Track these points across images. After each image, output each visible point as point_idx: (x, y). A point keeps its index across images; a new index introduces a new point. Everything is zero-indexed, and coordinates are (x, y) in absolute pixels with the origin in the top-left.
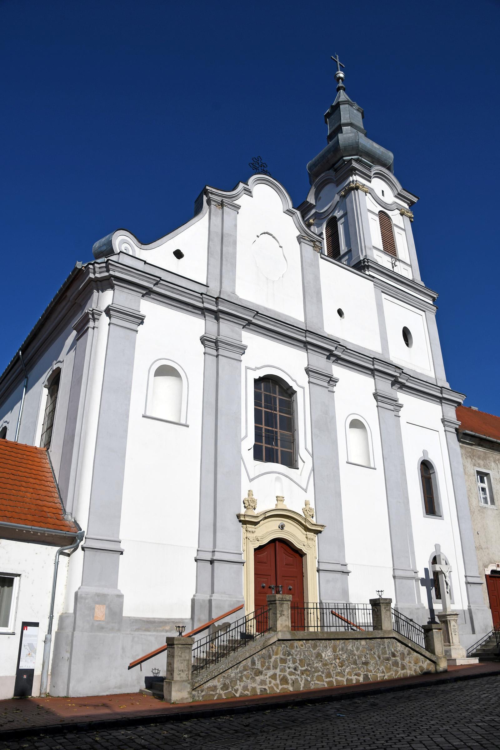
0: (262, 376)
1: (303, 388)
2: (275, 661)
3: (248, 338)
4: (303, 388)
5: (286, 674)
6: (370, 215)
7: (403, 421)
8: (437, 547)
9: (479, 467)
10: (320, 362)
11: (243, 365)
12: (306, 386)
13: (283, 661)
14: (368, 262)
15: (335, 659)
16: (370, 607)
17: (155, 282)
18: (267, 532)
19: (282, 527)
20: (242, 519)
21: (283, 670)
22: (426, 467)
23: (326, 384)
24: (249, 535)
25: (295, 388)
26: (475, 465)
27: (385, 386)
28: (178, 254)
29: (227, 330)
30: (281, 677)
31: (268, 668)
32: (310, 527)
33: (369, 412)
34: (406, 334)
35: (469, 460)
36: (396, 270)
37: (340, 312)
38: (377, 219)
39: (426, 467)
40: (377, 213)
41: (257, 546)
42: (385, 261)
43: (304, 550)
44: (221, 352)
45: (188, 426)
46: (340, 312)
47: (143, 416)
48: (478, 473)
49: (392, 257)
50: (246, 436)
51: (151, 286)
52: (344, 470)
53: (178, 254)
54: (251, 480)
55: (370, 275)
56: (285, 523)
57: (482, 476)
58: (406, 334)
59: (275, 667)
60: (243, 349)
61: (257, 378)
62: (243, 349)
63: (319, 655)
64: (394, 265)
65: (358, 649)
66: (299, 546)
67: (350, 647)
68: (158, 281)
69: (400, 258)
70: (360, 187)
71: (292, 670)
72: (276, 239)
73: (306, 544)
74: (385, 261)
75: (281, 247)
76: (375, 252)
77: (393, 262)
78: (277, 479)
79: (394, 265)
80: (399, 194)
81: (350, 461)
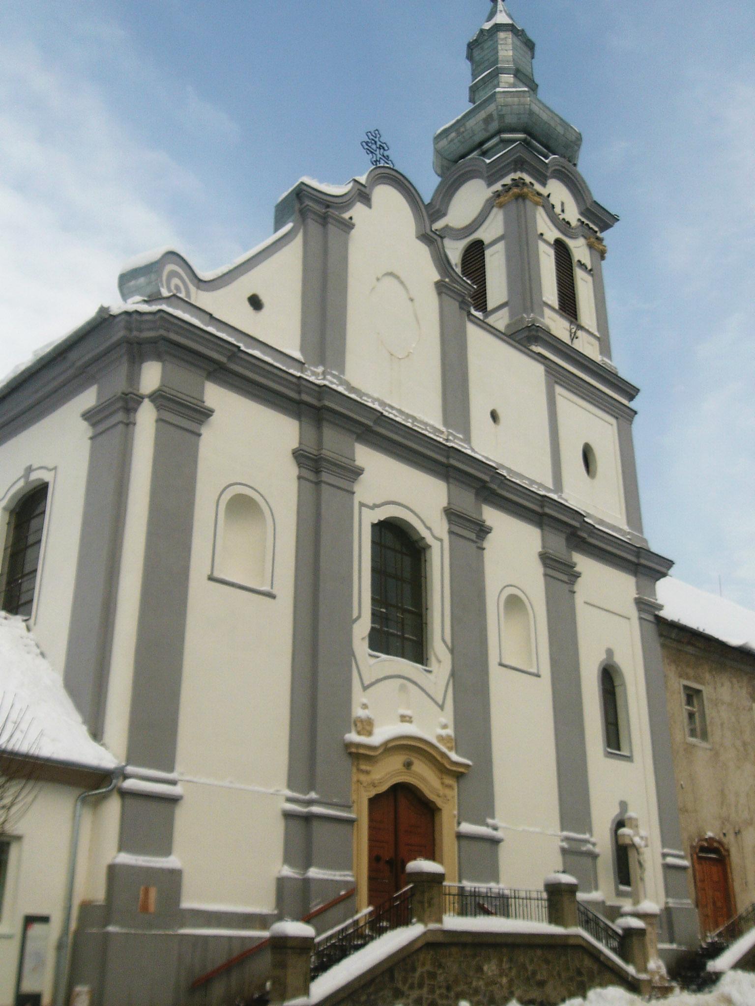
0: (382, 519)
1: (441, 540)
2: (422, 977)
3: (366, 456)
4: (441, 540)
5: (436, 996)
6: (542, 247)
7: (579, 599)
8: (623, 805)
9: (688, 678)
10: (467, 501)
11: (357, 499)
12: (446, 537)
13: (433, 975)
14: (537, 331)
15: (501, 975)
16: (545, 895)
17: (229, 354)
18: (386, 774)
19: (408, 765)
20: (353, 750)
21: (432, 991)
22: (609, 678)
23: (473, 536)
24: (363, 778)
25: (430, 540)
26: (681, 676)
27: (558, 544)
28: (255, 303)
29: (333, 441)
30: (429, 1001)
31: (412, 987)
32: (448, 766)
33: (532, 581)
34: (588, 456)
35: (673, 668)
36: (578, 345)
37: (494, 416)
38: (552, 252)
39: (609, 678)
40: (552, 242)
41: (373, 793)
42: (559, 326)
43: (439, 802)
44: (325, 477)
45: (273, 597)
46: (494, 416)
47: (211, 578)
48: (686, 688)
49: (571, 323)
50: (359, 617)
51: (223, 359)
52: (496, 674)
53: (255, 303)
54: (365, 688)
55: (539, 354)
56: (413, 759)
57: (692, 695)
58: (588, 456)
59: (421, 986)
60: (357, 472)
61: (376, 522)
62: (357, 472)
63: (480, 969)
64: (574, 337)
65: (532, 961)
66: (432, 797)
67: (521, 959)
68: (234, 352)
69: (583, 324)
70: (530, 195)
71: (444, 991)
72: (402, 283)
73: (441, 793)
74: (559, 326)
75: (412, 300)
76: (547, 311)
77: (573, 330)
78: (402, 688)
79: (574, 337)
80: (588, 210)
81: (217, 574)
